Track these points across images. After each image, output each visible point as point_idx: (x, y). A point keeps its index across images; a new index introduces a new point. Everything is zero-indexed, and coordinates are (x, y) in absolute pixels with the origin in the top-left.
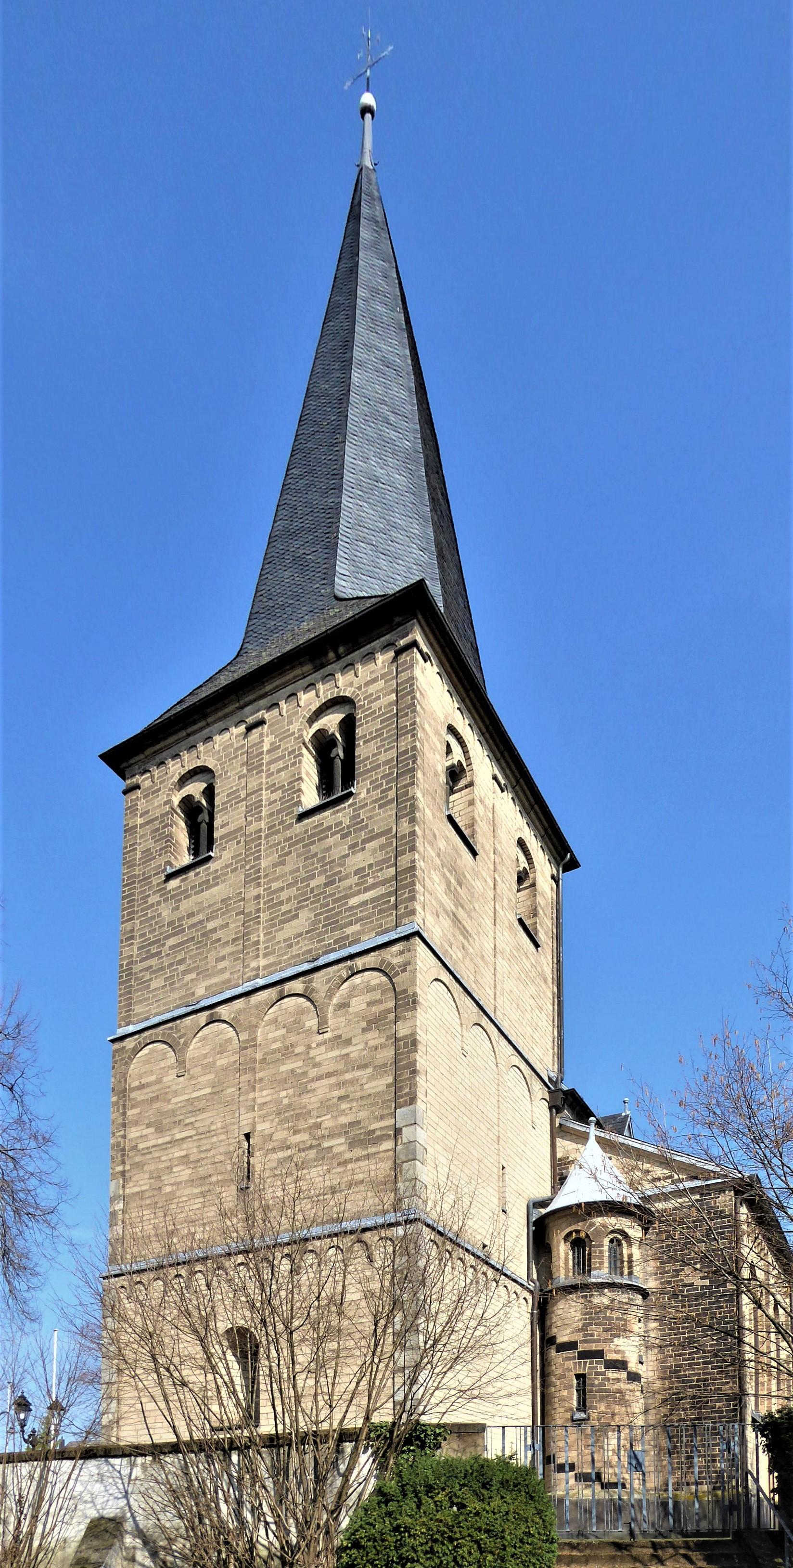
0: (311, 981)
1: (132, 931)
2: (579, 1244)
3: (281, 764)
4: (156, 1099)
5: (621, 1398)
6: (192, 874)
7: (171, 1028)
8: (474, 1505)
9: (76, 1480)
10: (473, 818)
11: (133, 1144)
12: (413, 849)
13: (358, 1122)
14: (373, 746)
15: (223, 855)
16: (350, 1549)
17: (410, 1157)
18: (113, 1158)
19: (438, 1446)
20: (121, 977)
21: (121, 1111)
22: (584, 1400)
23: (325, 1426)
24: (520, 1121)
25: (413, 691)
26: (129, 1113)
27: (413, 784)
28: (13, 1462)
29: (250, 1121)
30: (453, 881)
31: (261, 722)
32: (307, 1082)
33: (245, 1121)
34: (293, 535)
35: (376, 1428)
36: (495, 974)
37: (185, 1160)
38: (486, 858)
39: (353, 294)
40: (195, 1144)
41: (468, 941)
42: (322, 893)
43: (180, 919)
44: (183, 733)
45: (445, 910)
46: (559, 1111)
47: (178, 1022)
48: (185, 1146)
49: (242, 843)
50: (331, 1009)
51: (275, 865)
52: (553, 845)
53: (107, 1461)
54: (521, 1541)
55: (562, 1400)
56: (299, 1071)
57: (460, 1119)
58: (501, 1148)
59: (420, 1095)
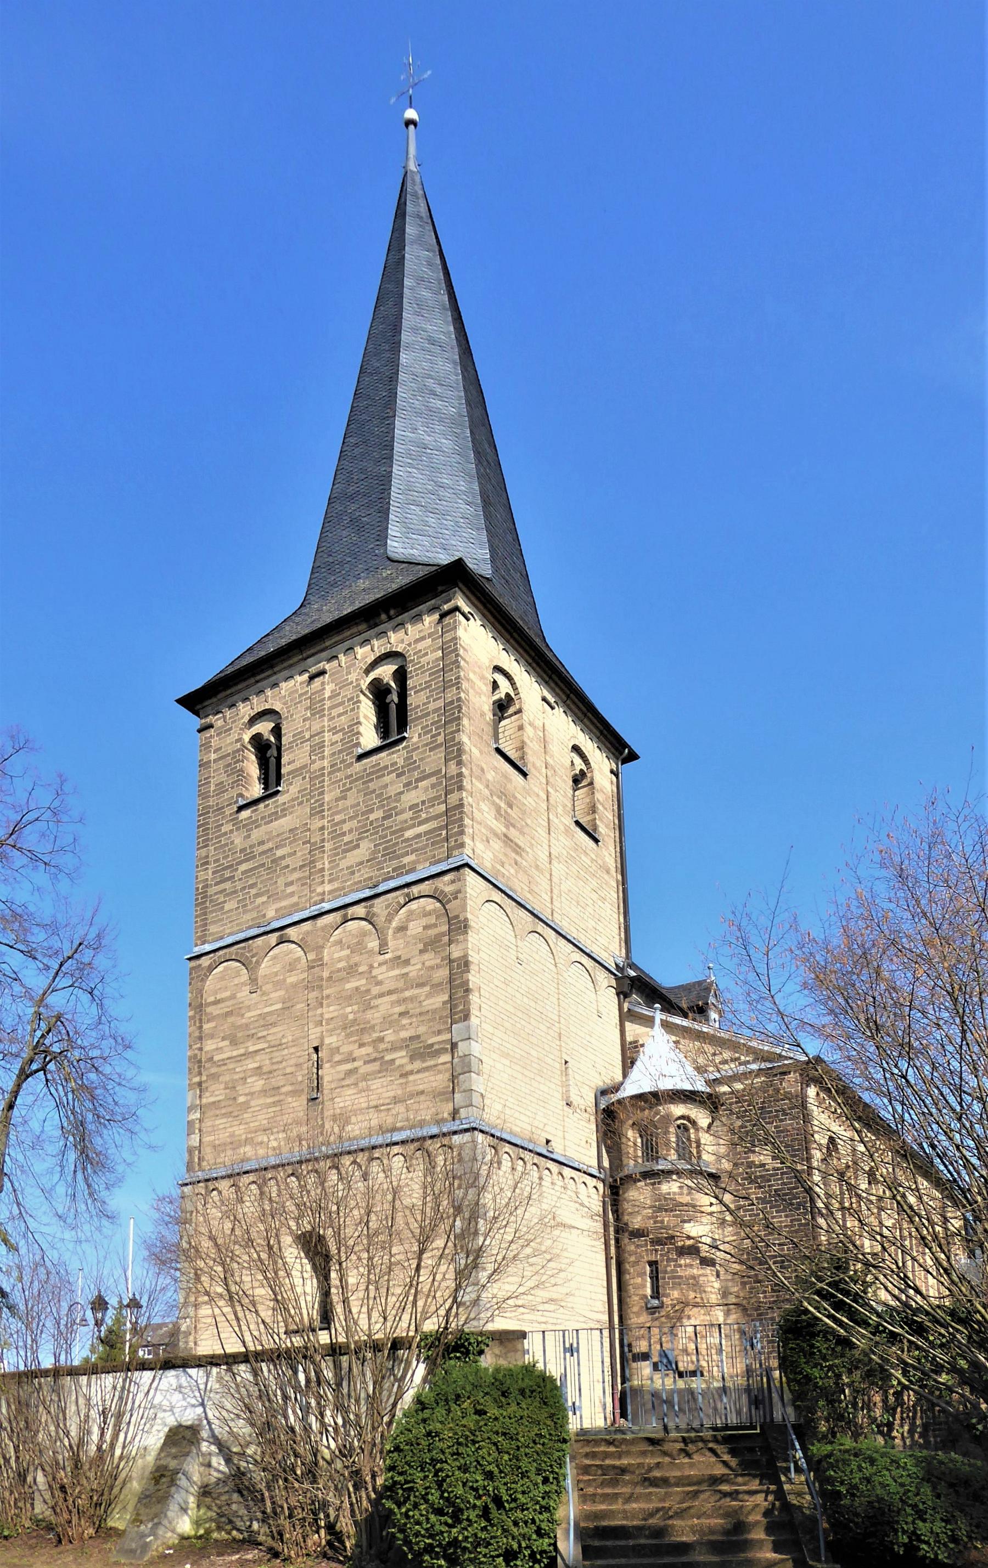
0: (372, 906)
1: (207, 857)
2: (644, 1131)
3: (341, 709)
4: (229, 1014)
5: (695, 1283)
6: (262, 805)
7: (244, 948)
8: (493, 1411)
9: (156, 1389)
10: (523, 742)
11: (209, 1056)
12: (461, 788)
13: (418, 1037)
14: (423, 696)
15: (290, 790)
16: (392, 1452)
17: (466, 1069)
18: (190, 1069)
19: (481, 1352)
20: (197, 899)
21: (198, 1025)
22: (658, 1287)
23: (380, 1336)
24: (584, 1013)
25: (456, 650)
26: (205, 1026)
27: (459, 730)
28: (96, 1373)
29: (318, 1035)
30: (503, 805)
31: (322, 673)
32: (371, 999)
33: (314, 1035)
34: (351, 498)
35: (425, 1337)
36: (551, 880)
37: (258, 1071)
38: (538, 774)
39: (401, 284)
40: (268, 1056)
41: (521, 856)
42: (380, 826)
43: (251, 847)
44: (252, 680)
45: (496, 835)
46: (626, 996)
47: (251, 942)
48: (258, 1058)
49: (307, 779)
50: (390, 932)
51: (337, 800)
52: (611, 743)
53: (185, 1371)
54: (534, 1442)
55: (637, 1287)
56: (363, 989)
57: (518, 1025)
58: (563, 1044)
59: (474, 1011)
